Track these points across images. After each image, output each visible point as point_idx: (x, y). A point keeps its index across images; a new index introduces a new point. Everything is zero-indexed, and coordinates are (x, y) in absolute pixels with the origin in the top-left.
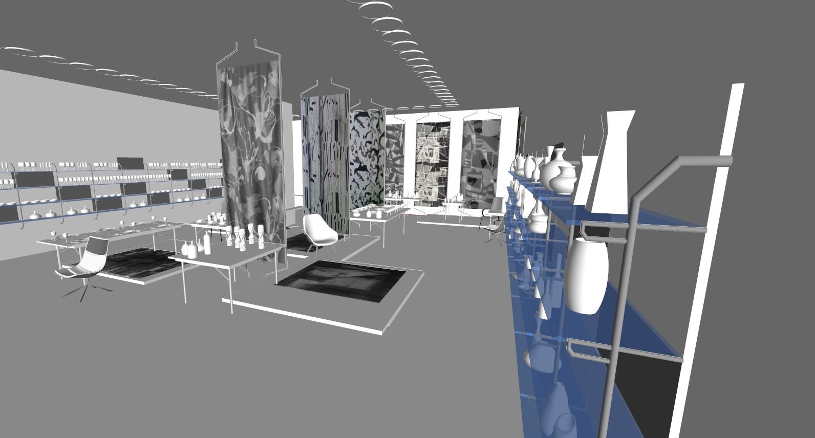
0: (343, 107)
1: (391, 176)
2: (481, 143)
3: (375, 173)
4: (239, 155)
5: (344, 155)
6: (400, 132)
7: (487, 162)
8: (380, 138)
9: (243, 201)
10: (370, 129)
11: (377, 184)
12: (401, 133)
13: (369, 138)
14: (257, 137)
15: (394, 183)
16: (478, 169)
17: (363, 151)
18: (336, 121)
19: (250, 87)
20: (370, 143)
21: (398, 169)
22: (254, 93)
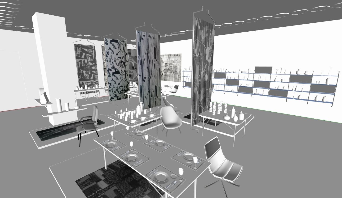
0: (158, 41)
1: (90, 76)
2: (131, 59)
3: (124, 75)
4: (200, 69)
5: (158, 66)
6: (92, 51)
7: (134, 67)
8: (125, 56)
9: (200, 93)
10: (119, 50)
11: (126, 81)
12: (93, 51)
13: (119, 55)
14: (206, 59)
15: (93, 80)
16: (132, 71)
17: (116, 62)
18: (155, 48)
19: (206, 34)
20: (120, 58)
21: (94, 72)
22: (207, 37)
